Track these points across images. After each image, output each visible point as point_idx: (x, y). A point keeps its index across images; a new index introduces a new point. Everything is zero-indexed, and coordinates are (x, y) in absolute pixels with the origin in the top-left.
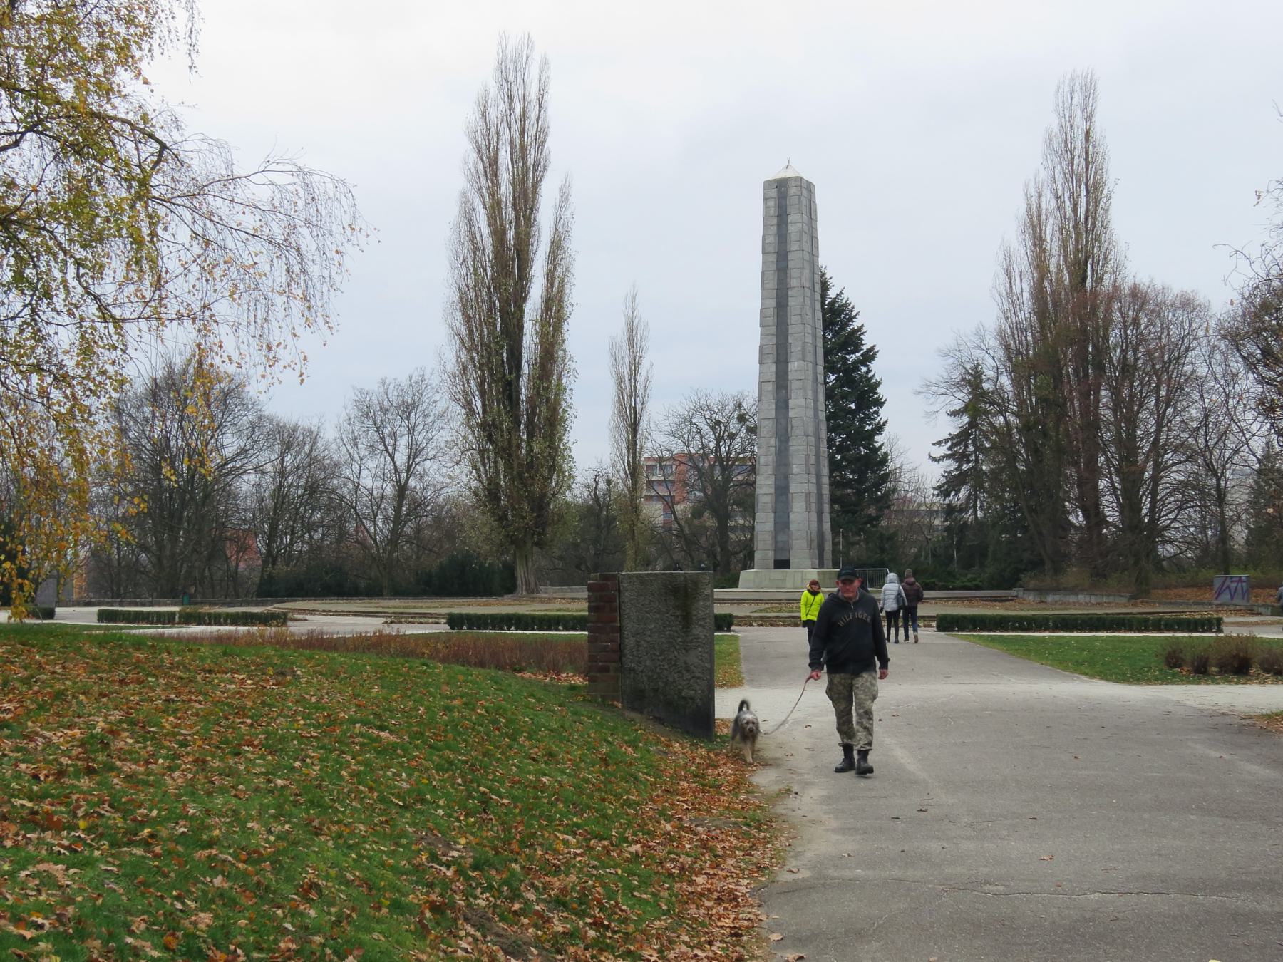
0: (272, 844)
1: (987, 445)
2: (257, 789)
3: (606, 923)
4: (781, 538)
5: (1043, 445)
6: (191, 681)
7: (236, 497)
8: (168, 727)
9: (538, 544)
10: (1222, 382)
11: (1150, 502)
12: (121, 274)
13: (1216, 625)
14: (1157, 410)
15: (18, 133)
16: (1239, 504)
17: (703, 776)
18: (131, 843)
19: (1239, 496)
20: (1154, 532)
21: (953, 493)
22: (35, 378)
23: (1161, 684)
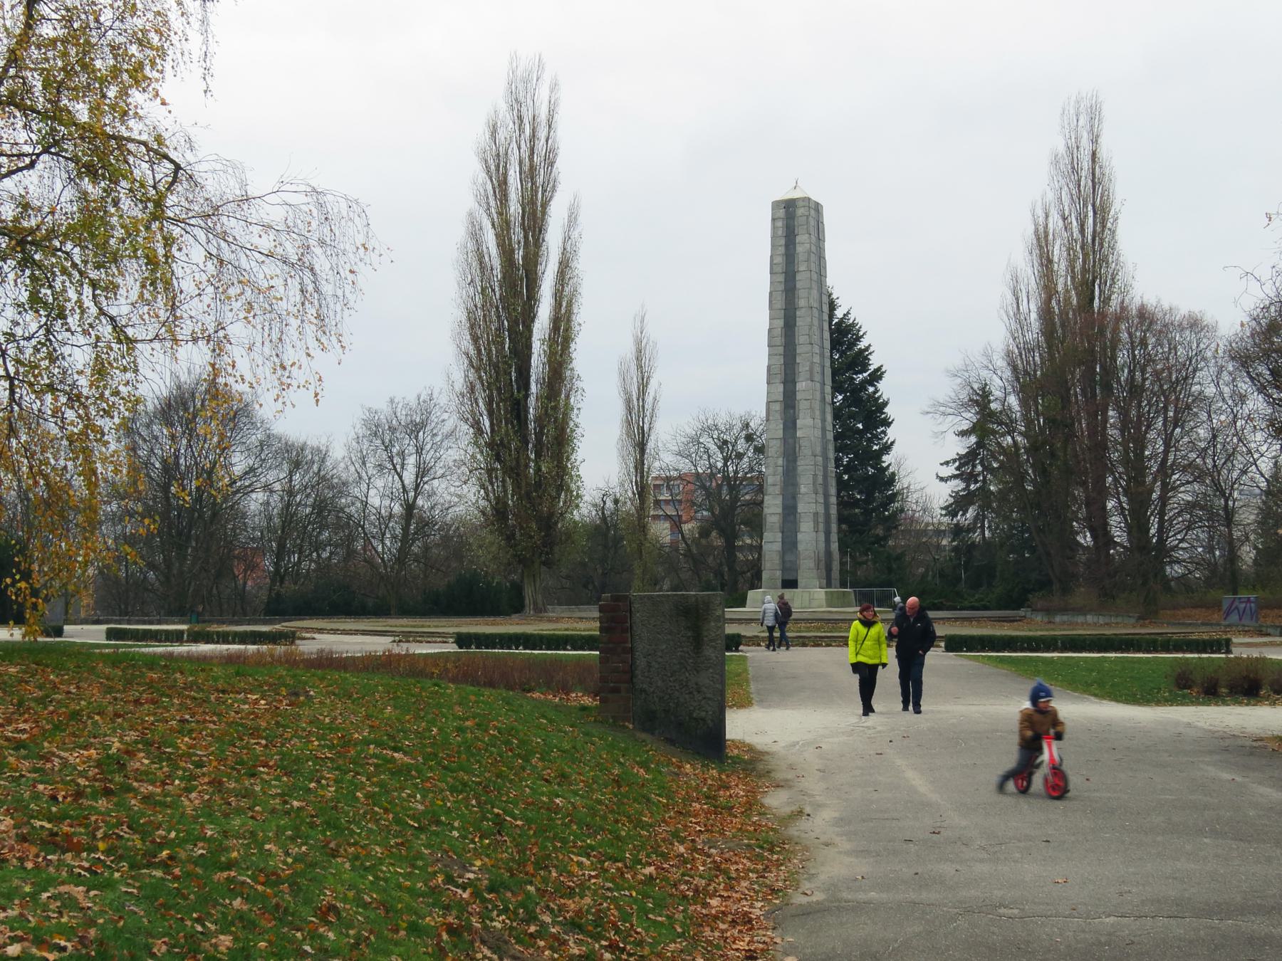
0: (289, 866)
1: (995, 465)
2: (273, 811)
3: (622, 945)
4: (789, 557)
5: (1051, 465)
6: (204, 701)
7: (244, 515)
8: (183, 747)
9: (547, 563)
10: (1230, 402)
11: (1158, 522)
12: (134, 295)
13: (1225, 646)
14: (1165, 430)
15: (33, 154)
16: (1249, 524)
17: (715, 798)
18: (150, 865)
19: (1248, 517)
20: (1163, 552)
21: (961, 513)
22: (49, 398)
23: (1171, 705)
